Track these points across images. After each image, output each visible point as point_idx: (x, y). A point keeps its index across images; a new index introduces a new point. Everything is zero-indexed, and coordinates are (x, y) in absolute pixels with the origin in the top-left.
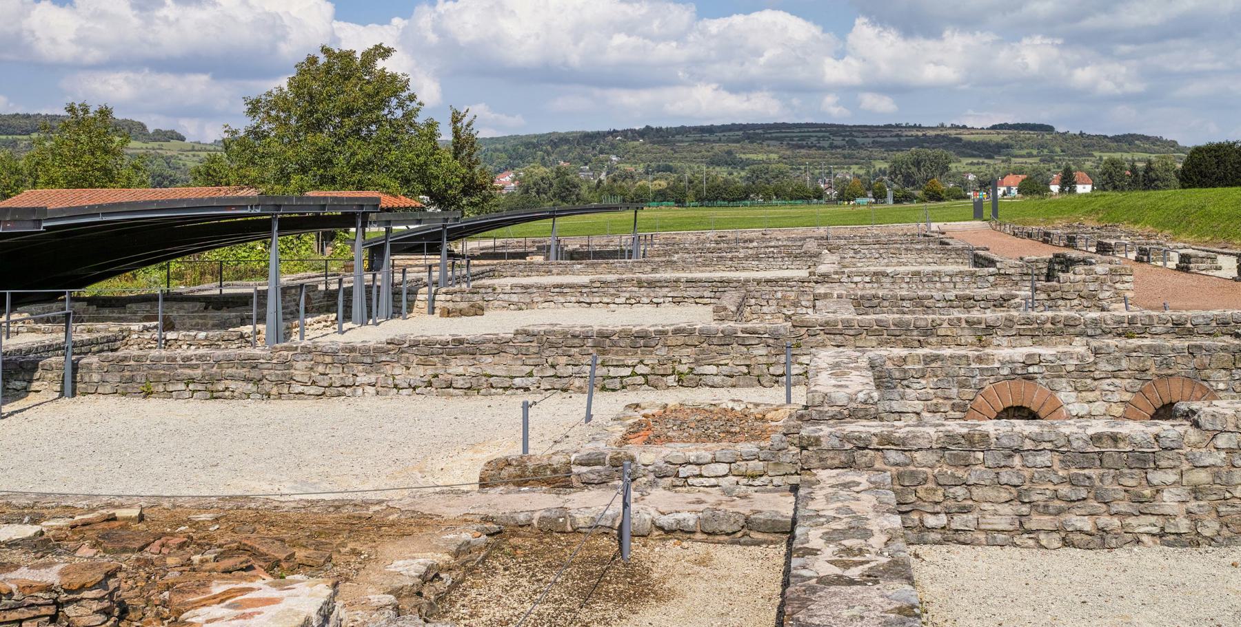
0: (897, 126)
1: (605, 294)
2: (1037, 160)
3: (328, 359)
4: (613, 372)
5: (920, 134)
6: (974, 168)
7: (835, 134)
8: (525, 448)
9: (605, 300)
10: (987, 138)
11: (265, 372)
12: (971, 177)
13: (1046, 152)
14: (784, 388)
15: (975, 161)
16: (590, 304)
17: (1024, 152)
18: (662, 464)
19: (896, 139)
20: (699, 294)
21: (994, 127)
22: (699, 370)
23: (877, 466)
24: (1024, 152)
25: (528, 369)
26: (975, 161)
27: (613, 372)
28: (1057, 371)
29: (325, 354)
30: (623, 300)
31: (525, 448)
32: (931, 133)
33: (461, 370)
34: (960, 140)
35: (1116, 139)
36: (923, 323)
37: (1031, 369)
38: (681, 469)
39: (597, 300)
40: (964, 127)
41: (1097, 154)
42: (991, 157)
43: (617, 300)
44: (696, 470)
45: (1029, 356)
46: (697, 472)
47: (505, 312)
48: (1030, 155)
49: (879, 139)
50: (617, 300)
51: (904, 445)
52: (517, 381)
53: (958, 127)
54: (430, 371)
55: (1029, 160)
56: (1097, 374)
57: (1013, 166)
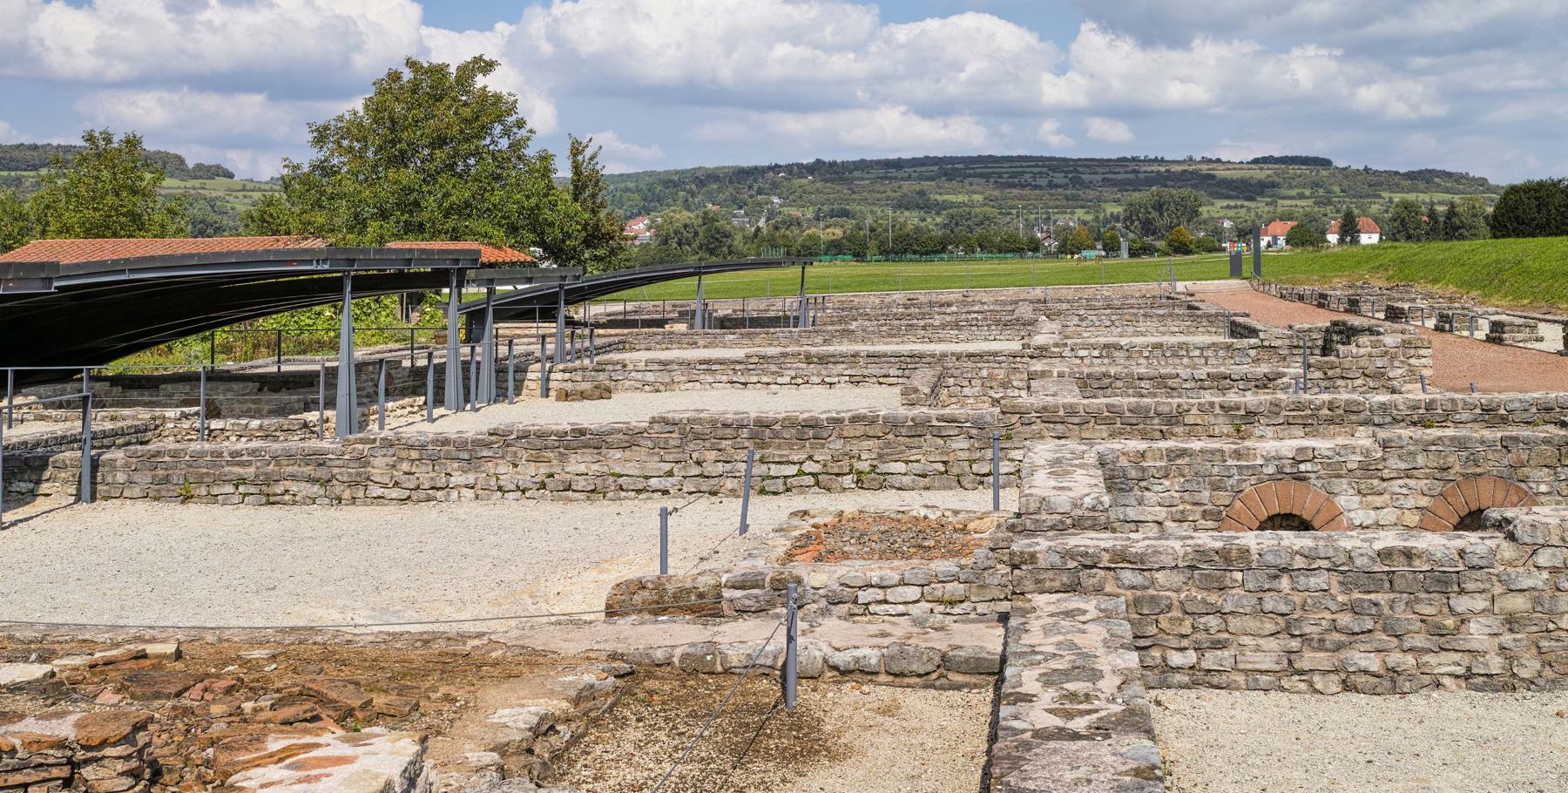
0: (1134, 159)
1: (764, 372)
2: (1310, 202)
3: (414, 454)
4: (775, 470)
5: (1162, 169)
6: (1231, 213)
7: (1055, 169)
8: (664, 566)
9: (765, 379)
10: (1247, 174)
11: (335, 471)
12: (1227, 224)
13: (1321, 192)
14: (991, 491)
15: (1232, 203)
16: (745, 384)
17: (1294, 192)
18: (836, 587)
19: (1132, 176)
20: (883, 372)
21: (1256, 161)
22: (883, 468)
23: (1108, 589)
24: (1294, 192)
25: (667, 467)
26: (1232, 203)
27: (775, 470)
28: (1335, 469)
29: (411, 447)
30: (787, 379)
31: (664, 566)
32: (1177, 168)
33: (582, 468)
34: (1213, 177)
35: (1411, 176)
36: (1166, 409)
37: (1302, 467)
38: (860, 593)
39: (755, 379)
40: (1219, 161)
41: (1386, 195)
42: (1252, 199)
43: (780, 380)
44: (880, 594)
45: (1301, 450)
46: (881, 597)
47: (638, 394)
48: (1301, 197)
49: (1110, 176)
50: (780, 380)
51: (1142, 562)
52: (654, 482)
53: (1210, 161)
54: (543, 469)
55: (1300, 203)
56: (1386, 474)
57: (1279, 210)
